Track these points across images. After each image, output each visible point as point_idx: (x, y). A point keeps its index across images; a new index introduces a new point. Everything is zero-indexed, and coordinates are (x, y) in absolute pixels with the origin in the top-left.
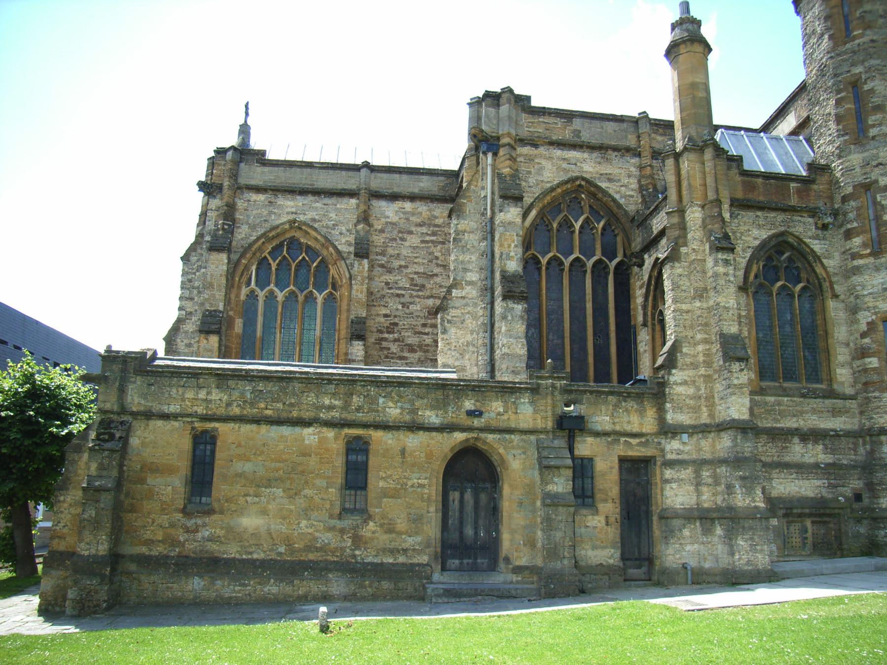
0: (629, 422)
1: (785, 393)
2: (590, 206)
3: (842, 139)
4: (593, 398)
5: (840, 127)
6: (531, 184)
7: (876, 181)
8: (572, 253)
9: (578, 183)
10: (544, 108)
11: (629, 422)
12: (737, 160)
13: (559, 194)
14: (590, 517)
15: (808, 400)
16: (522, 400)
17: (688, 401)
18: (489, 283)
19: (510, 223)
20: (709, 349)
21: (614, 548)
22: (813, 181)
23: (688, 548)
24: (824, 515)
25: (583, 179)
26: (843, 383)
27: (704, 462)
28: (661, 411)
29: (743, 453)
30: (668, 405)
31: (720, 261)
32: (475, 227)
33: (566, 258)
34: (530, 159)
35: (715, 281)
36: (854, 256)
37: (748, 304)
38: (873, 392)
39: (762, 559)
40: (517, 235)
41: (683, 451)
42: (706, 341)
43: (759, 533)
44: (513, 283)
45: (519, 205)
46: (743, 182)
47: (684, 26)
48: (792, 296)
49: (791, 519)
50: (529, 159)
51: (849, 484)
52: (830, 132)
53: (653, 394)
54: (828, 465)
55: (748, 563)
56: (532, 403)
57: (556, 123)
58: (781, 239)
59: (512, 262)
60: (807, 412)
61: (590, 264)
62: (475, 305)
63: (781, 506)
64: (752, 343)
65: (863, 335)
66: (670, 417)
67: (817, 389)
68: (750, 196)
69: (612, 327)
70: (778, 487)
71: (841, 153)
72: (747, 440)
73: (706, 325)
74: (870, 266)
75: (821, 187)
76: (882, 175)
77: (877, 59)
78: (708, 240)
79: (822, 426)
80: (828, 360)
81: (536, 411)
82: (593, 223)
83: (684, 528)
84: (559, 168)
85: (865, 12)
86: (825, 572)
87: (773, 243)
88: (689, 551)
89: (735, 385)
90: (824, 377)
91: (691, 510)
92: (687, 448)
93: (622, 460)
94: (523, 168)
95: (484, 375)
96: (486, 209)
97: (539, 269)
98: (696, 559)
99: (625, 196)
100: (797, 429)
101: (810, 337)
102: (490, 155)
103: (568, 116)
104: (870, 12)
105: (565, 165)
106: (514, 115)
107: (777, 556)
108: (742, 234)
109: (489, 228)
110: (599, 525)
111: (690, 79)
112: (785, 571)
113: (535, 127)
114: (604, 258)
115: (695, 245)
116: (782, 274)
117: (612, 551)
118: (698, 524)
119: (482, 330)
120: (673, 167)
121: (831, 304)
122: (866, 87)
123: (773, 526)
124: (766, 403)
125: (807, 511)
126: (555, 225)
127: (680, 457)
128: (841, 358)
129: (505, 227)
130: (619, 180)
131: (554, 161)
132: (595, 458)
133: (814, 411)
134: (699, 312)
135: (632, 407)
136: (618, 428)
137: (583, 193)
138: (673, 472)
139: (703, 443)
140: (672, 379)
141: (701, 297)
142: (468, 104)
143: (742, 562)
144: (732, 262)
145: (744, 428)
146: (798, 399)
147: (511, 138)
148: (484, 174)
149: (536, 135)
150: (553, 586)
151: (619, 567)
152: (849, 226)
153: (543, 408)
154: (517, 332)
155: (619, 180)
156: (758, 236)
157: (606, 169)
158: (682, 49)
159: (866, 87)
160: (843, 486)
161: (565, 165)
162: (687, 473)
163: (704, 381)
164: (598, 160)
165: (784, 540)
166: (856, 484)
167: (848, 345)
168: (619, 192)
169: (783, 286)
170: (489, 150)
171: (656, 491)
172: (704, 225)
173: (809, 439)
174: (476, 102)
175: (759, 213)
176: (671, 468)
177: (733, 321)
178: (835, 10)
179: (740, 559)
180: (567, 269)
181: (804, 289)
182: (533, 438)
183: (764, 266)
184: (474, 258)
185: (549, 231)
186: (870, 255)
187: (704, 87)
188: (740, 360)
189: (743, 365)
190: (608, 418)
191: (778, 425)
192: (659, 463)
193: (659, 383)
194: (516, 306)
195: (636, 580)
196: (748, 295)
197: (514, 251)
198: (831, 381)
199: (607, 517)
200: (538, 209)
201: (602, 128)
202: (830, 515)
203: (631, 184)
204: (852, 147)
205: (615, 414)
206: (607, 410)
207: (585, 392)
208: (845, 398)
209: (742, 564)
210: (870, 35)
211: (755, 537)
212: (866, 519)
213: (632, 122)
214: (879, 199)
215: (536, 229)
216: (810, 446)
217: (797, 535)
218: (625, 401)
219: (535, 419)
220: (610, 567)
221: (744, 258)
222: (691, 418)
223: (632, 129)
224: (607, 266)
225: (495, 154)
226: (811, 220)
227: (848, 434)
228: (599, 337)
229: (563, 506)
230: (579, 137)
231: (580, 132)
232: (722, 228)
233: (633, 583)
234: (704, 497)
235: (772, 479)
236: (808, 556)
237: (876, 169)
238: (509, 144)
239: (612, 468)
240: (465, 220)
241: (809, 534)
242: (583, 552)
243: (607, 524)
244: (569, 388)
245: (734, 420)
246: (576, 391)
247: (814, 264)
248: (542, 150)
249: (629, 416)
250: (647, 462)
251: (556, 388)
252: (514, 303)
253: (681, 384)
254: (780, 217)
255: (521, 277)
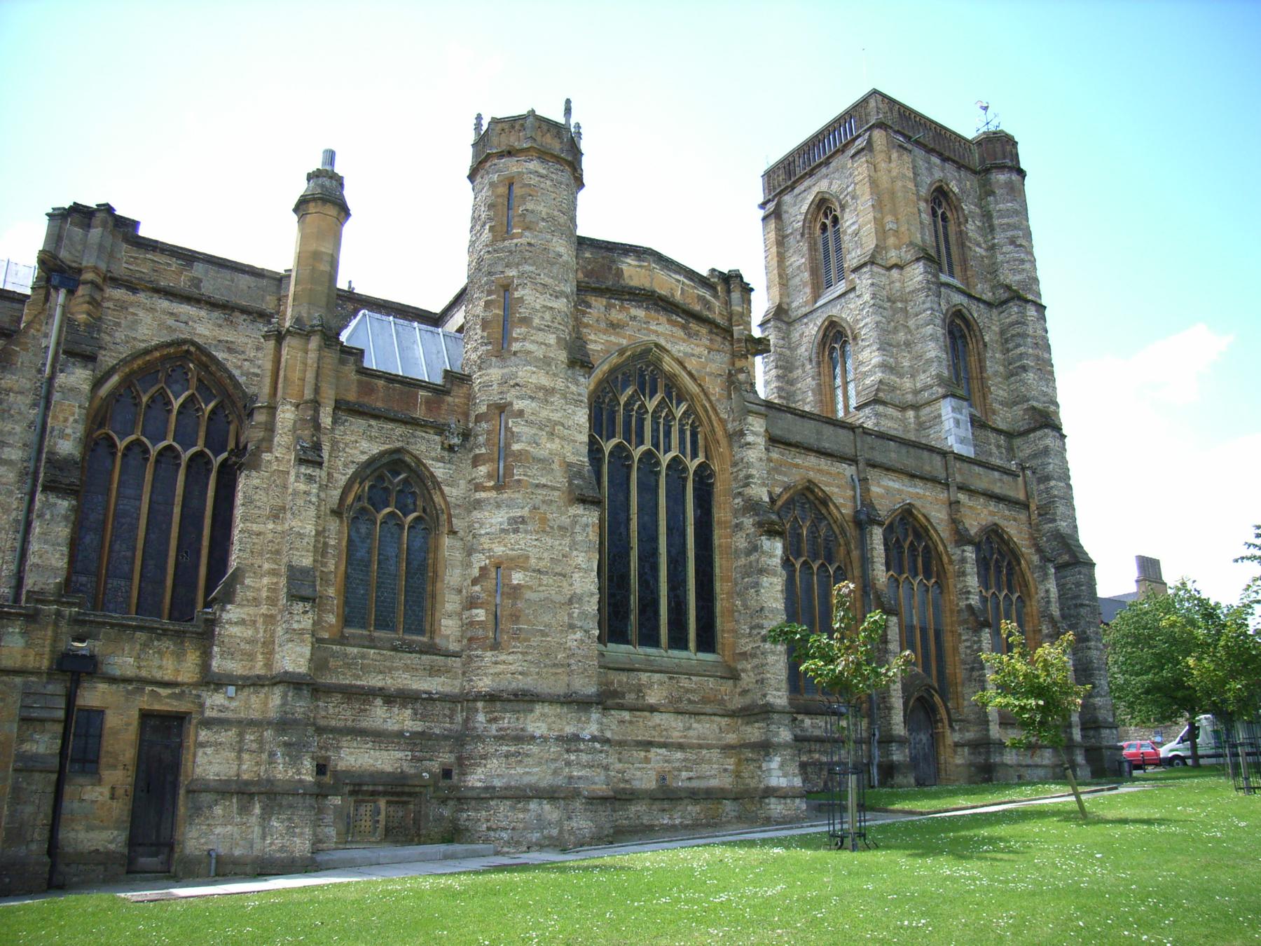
0: (160, 667)
1: (372, 643)
2: (199, 380)
3: (484, 348)
4: (113, 632)
5: (485, 334)
6: (118, 340)
7: (511, 404)
8: (164, 439)
9: (185, 348)
10: (156, 242)
11: (160, 667)
12: (356, 354)
13: (156, 358)
14: (89, 787)
15: (400, 654)
16: (11, 630)
17: (243, 645)
18: (31, 465)
19: (72, 390)
20: (276, 583)
21: (117, 828)
22: (448, 393)
23: (218, 830)
24: (403, 794)
25: (193, 343)
26: (447, 637)
27: (252, 723)
28: (206, 655)
29: (293, 714)
30: (216, 649)
31: (302, 476)
32: (28, 386)
33: (154, 446)
34: (122, 307)
35: (292, 500)
36: (479, 487)
37: (340, 532)
38: (476, 649)
39: (301, 846)
40: (79, 407)
41: (227, 708)
42: (273, 573)
43: (300, 813)
44: (61, 470)
45: (90, 366)
46: (359, 382)
47: (320, 181)
48: (401, 527)
49: (360, 797)
50: (121, 307)
51: (437, 757)
52: (476, 337)
53: (198, 633)
54: (415, 734)
55: (282, 849)
56: (24, 633)
57: (169, 265)
58: (395, 457)
59: (66, 442)
60: (397, 669)
61: (186, 456)
62: (10, 493)
63: (347, 781)
64: (338, 580)
65: (475, 582)
66: (216, 664)
67: (414, 641)
68: (366, 400)
69: (206, 542)
70: (348, 758)
71: (482, 364)
72: (300, 698)
73: (278, 552)
74: (492, 501)
75: (457, 400)
76: (517, 397)
77: (532, 265)
78: (295, 449)
79: (415, 687)
80: (433, 607)
81: (28, 645)
82: (199, 403)
83: (216, 805)
84: (162, 325)
85: (527, 210)
86: (381, 861)
87: (384, 460)
88: (219, 834)
89: (294, 630)
90: (428, 627)
91: (228, 782)
92: (234, 704)
93: (145, 716)
94: (110, 317)
95: (7, 590)
96: (44, 365)
97: (114, 454)
98: (228, 844)
99: (247, 374)
100: (381, 689)
101: (419, 579)
102: (63, 293)
103: (188, 257)
104: (532, 212)
105: (171, 322)
106: (108, 244)
107: (336, 843)
108: (346, 445)
109: (44, 391)
110: (100, 798)
111: (313, 246)
112: (332, 860)
113: (137, 265)
114: (207, 451)
115: (278, 452)
116: (393, 500)
117: (116, 833)
118: (234, 800)
119: (12, 529)
120: (272, 352)
121: (447, 541)
122: (517, 295)
123: (335, 806)
124: (346, 655)
125: (381, 788)
126: (145, 399)
127: (222, 715)
128: (449, 607)
129: (63, 393)
130: (243, 352)
131: (156, 314)
132: (108, 712)
133: (407, 668)
134: (270, 536)
135: (168, 648)
136: (144, 673)
137: (193, 362)
138: (210, 733)
139: (253, 698)
140: (225, 616)
141: (276, 517)
142: (48, 215)
143: (274, 847)
144: (318, 479)
145: (298, 683)
146: (389, 653)
147: (98, 274)
148: (51, 316)
149: (137, 275)
150: (7, 880)
151: (123, 855)
152: (477, 451)
153: (40, 641)
154: (57, 537)
155: (243, 352)
156: (366, 450)
157: (228, 335)
158: (312, 208)
159: (517, 295)
160: (430, 760)
161: (171, 322)
162: (228, 736)
163: (264, 622)
164: (220, 322)
165: (348, 824)
166: (446, 757)
167: (460, 591)
168: (240, 367)
169: (392, 514)
170: (62, 285)
171: (186, 757)
172: (294, 430)
173: (395, 702)
174: (58, 215)
175: (373, 422)
176: (208, 729)
177: (308, 551)
178: (500, 200)
179: (271, 844)
180: (152, 459)
181: (418, 519)
182: (18, 680)
183: (371, 487)
184: (18, 429)
185: (136, 405)
186: (493, 488)
187: (329, 259)
188: (304, 599)
189: (308, 606)
190: (131, 660)
191: (359, 683)
192: (194, 721)
193: (207, 620)
194: (60, 502)
195: (146, 872)
196: (342, 521)
197: (73, 428)
198: (432, 632)
199: (113, 788)
200: (122, 374)
201: (232, 281)
202: (410, 794)
203: (258, 359)
204: (494, 359)
205: (142, 656)
206: (132, 649)
207: (104, 624)
208: (448, 654)
209: (274, 850)
210: (528, 237)
211: (295, 817)
212: (452, 799)
213: (274, 279)
214: (510, 424)
215: (118, 401)
216: (396, 710)
217: (368, 818)
218: (159, 640)
219: (25, 656)
220: (108, 854)
221: (345, 475)
222: (244, 667)
223: (274, 289)
224: (209, 462)
225: (71, 292)
226: (437, 438)
227: (445, 698)
228: (186, 553)
229: (41, 771)
230: (198, 288)
231: (201, 281)
232: (313, 436)
233: (138, 876)
234: (244, 767)
235: (341, 748)
236: (377, 843)
237: (513, 389)
238: (92, 282)
239: (128, 724)
240: (13, 374)
241: (382, 817)
242: (72, 835)
243: (113, 797)
244: (81, 618)
245: (286, 673)
246: (92, 622)
247: (433, 491)
248: (142, 297)
249: (161, 660)
250: (180, 719)
251: (63, 617)
252: (58, 497)
253: (236, 623)
254: (399, 430)
255: (76, 463)
